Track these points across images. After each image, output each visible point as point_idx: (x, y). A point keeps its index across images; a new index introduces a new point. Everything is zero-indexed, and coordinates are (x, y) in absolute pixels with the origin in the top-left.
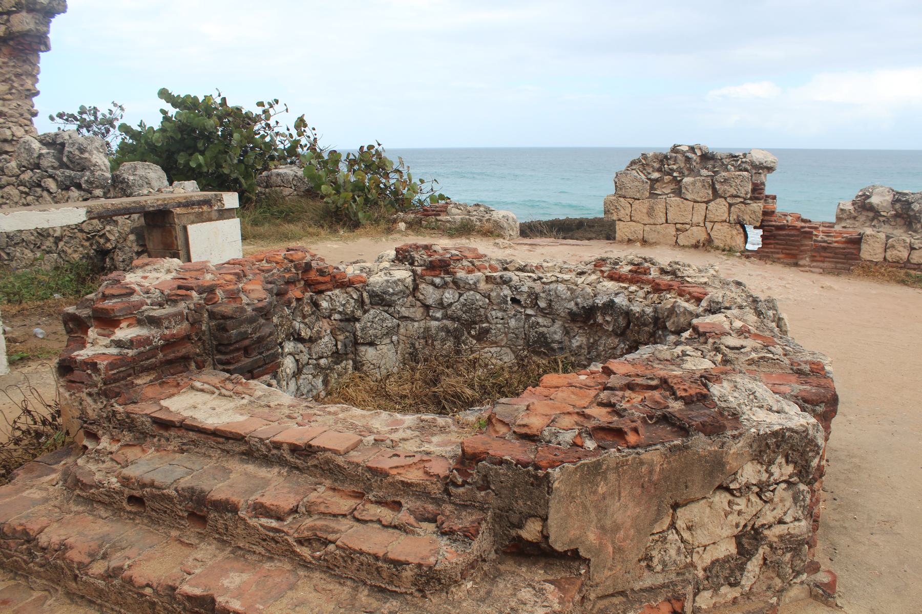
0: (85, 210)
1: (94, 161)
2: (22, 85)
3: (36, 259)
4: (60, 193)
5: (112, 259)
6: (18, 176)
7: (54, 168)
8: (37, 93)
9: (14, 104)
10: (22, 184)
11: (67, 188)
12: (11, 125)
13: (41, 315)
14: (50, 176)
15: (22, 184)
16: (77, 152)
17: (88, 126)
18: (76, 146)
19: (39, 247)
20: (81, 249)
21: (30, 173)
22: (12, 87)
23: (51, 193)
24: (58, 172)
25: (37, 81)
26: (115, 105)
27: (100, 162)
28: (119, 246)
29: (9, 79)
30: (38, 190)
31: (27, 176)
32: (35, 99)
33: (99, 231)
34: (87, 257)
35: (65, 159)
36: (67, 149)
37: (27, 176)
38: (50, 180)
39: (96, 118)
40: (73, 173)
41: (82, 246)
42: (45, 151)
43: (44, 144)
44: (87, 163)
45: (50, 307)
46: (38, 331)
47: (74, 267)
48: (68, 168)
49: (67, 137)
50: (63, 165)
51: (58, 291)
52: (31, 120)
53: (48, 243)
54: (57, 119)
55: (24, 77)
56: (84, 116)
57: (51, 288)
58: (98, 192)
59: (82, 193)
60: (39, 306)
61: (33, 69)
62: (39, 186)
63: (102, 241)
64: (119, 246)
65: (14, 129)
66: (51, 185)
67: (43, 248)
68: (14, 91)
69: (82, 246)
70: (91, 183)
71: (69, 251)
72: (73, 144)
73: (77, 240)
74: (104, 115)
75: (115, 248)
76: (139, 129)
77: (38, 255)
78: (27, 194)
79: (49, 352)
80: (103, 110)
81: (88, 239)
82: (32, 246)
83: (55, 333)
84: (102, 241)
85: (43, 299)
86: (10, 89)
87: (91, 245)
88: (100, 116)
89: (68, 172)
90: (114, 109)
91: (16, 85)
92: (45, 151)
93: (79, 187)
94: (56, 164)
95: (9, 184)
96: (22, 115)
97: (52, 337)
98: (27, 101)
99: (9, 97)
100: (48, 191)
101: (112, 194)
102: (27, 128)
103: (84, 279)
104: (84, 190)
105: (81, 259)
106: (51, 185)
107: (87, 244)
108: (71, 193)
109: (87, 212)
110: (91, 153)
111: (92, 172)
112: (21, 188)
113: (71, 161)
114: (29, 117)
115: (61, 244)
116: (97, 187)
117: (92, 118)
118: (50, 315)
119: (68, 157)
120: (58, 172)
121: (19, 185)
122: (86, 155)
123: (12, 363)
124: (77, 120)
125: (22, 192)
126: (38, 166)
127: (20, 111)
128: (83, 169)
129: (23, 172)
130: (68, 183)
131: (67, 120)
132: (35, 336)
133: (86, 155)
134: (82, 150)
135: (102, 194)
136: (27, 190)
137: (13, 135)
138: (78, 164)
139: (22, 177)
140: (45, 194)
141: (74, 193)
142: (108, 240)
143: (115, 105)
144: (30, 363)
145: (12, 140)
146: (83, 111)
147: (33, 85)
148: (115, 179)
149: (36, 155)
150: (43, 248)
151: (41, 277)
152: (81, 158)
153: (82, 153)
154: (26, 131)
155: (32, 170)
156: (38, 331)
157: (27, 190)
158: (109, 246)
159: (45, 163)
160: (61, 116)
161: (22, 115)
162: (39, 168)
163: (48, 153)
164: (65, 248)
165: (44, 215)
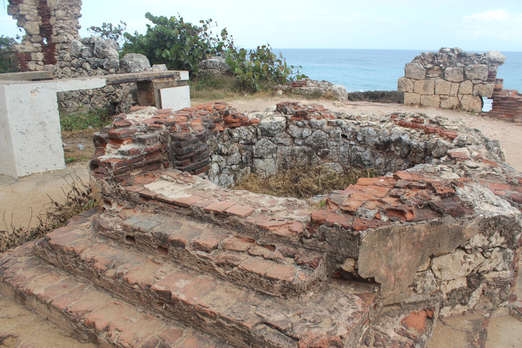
0: (105, 80)
1: (110, 53)
2: (73, 12)
3: (79, 107)
4: (92, 71)
5: (120, 107)
6: (71, 61)
7: (89, 57)
8: (81, 16)
9: (68, 22)
10: (73, 66)
11: (96, 68)
12: (67, 34)
13: (82, 137)
14: (87, 62)
15: (73, 66)
16: (101, 48)
17: (107, 34)
18: (101, 45)
19: (81, 101)
20: (103, 102)
21: (76, 60)
22: (68, 13)
23: (88, 71)
24: (91, 59)
25: (80, 9)
26: (122, 22)
27: (113, 54)
28: (123, 100)
29: (66, 8)
30: (81, 69)
31: (75, 61)
32: (79, 19)
33: (112, 92)
34: (106, 106)
35: (95, 52)
36: (96, 46)
37: (75, 61)
38: (87, 63)
39: (111, 29)
40: (99, 60)
41: (104, 100)
42: (84, 47)
43: (84, 44)
44: (106, 54)
45: (86, 133)
46: (80, 146)
47: (99, 111)
48: (96, 57)
49: (96, 40)
50: (94, 55)
51: (91, 124)
52: (77, 31)
53: (86, 99)
54: (91, 30)
55: (74, 7)
56: (105, 29)
57: (87, 123)
58: (112, 70)
59: (104, 71)
60: (81, 133)
61: (78, 3)
62: (81, 67)
63: (114, 97)
64: (123, 100)
65: (69, 36)
66: (87, 66)
67: (83, 101)
68: (68, 15)
69: (104, 100)
70: (109, 65)
71: (97, 103)
72: (99, 43)
73: (101, 97)
74: (115, 28)
75: (121, 101)
76: (135, 36)
77: (81, 105)
78: (75, 71)
79: (86, 158)
80: (115, 25)
81: (107, 96)
82: (77, 100)
83: (89, 147)
84: (114, 97)
85: (83, 129)
86: (67, 14)
87: (108, 100)
88: (113, 29)
89: (96, 59)
90: (121, 25)
91: (69, 11)
92: (84, 47)
93: (102, 67)
94: (90, 55)
95: (65, 66)
96: (72, 28)
97: (88, 150)
98: (75, 20)
99: (66, 18)
100: (86, 70)
101: (120, 71)
102: (75, 35)
103: (104, 118)
104: (105, 69)
105: (103, 107)
106: (87, 66)
107: (106, 99)
108: (98, 71)
109: (107, 81)
110: (108, 49)
111: (109, 59)
112: (72, 68)
113: (98, 53)
114: (77, 29)
115: (93, 99)
116: (112, 68)
117: (109, 30)
118: (86, 138)
119: (96, 50)
120: (91, 59)
121: (71, 67)
122: (106, 50)
123: (67, 163)
124: (101, 31)
125: (72, 70)
126: (81, 56)
127: (72, 26)
128: (104, 58)
129: (73, 59)
130: (96, 65)
131: (96, 31)
132: (79, 149)
133: (106, 50)
134: (104, 47)
135: (114, 71)
136: (75, 69)
137: (68, 40)
138: (102, 55)
139: (72, 62)
140: (84, 71)
141: (100, 71)
142: (117, 97)
143: (122, 22)
144: (76, 163)
145: (68, 42)
146: (104, 26)
147: (79, 11)
148: (121, 63)
149: (80, 50)
150: (83, 101)
151: (82, 117)
152: (104, 52)
153: (104, 49)
154: (75, 37)
155: (78, 58)
156: (80, 146)
157: (75, 69)
158: (118, 100)
159: (84, 54)
160: (93, 28)
161: (72, 28)
162: (81, 57)
163: (86, 49)
164: (95, 101)
165: (84, 82)
